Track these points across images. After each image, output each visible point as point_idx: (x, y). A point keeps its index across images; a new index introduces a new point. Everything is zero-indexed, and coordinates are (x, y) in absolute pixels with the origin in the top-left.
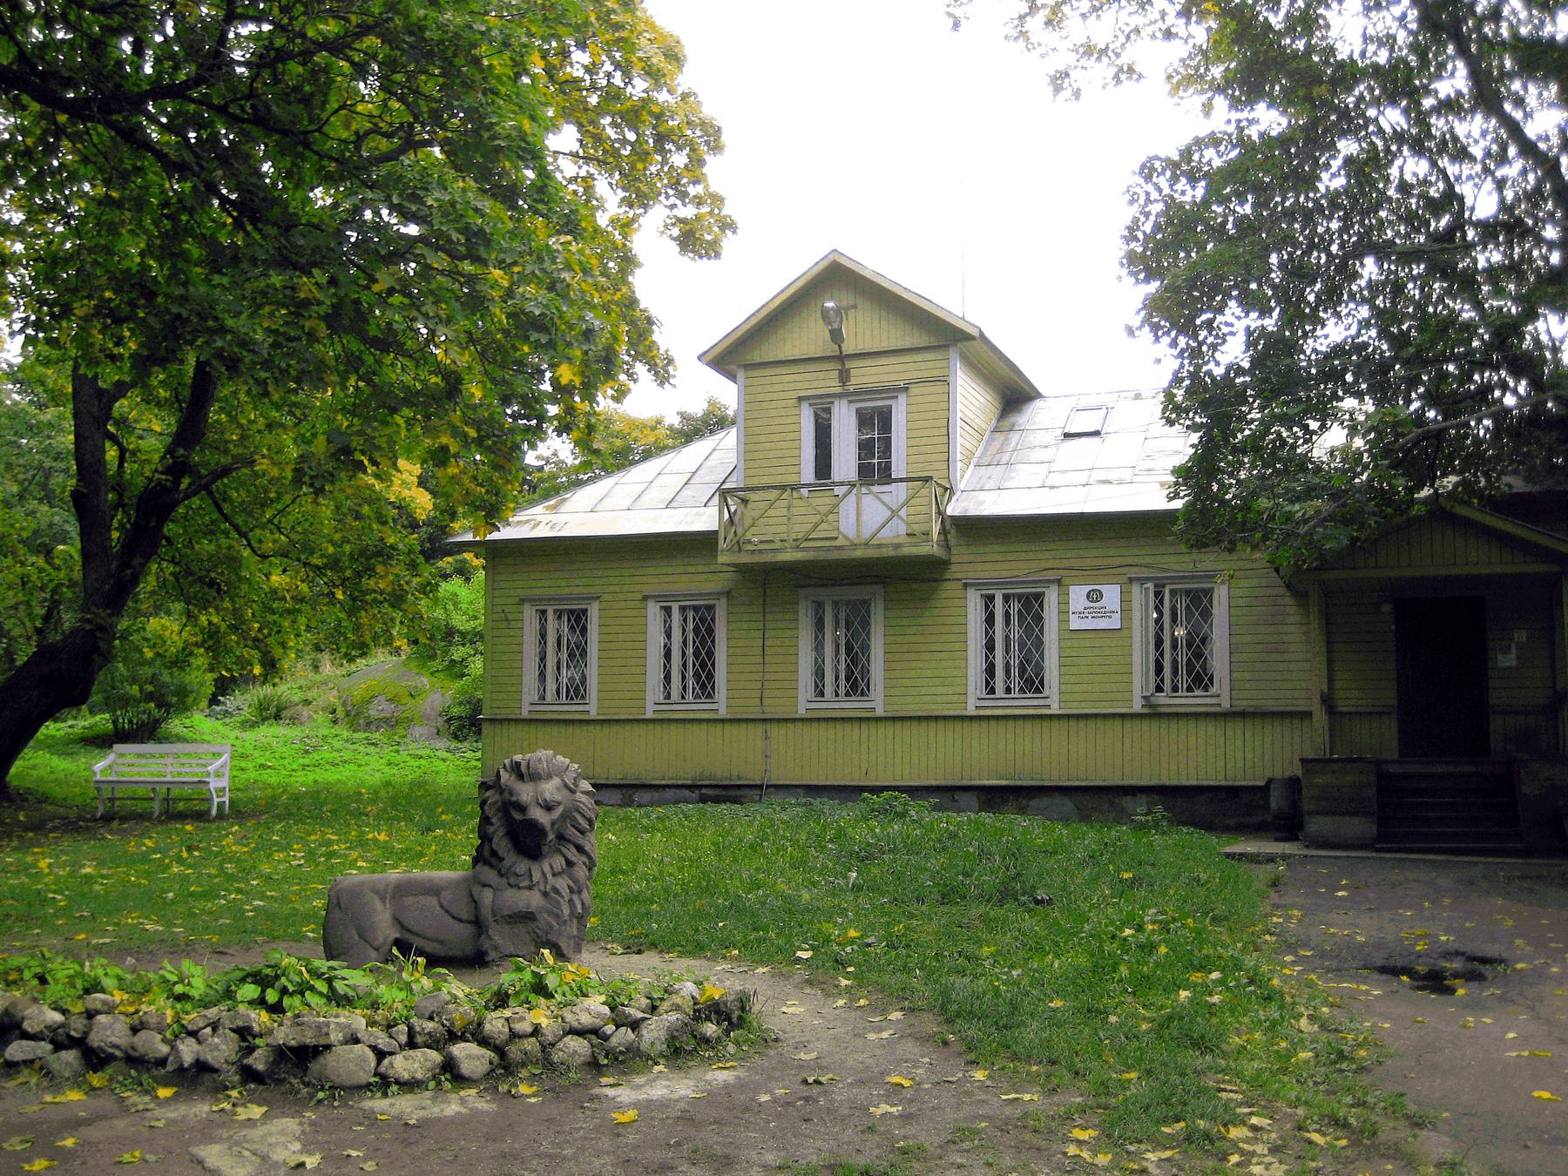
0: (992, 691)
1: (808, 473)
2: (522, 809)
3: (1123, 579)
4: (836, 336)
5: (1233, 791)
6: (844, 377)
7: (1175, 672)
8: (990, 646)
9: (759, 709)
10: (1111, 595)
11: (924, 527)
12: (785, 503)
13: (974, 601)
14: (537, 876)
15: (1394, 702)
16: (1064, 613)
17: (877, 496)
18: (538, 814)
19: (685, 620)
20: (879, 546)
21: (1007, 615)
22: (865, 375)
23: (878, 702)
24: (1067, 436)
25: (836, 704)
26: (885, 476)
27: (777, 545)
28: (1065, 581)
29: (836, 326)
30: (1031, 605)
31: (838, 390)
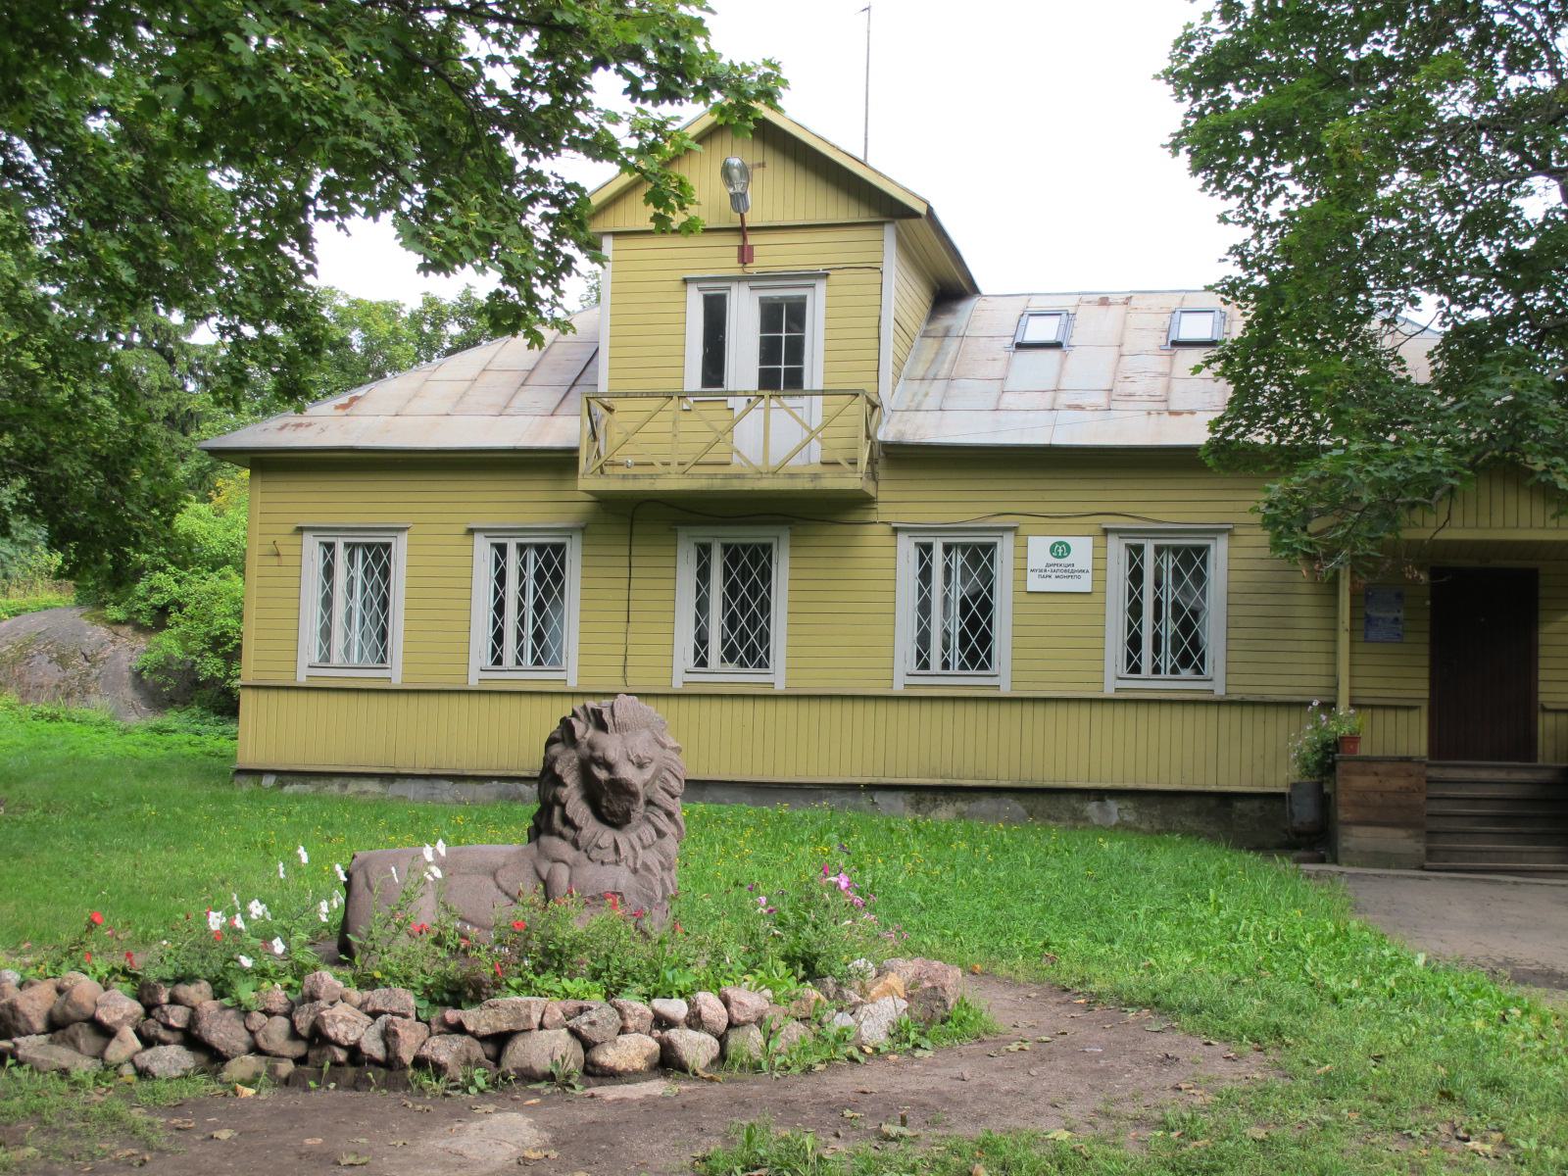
0: (926, 666)
1: (693, 379)
2: (609, 767)
3: (1094, 529)
4: (738, 201)
5: (1226, 798)
6: (745, 255)
7: (1157, 648)
8: (925, 608)
9: (621, 681)
10: (1082, 549)
11: (850, 454)
12: (669, 416)
13: (907, 550)
14: (624, 848)
15: (1426, 695)
16: (1022, 570)
17: (790, 410)
18: (627, 772)
19: (524, 563)
20: (792, 476)
21: (947, 570)
22: (770, 253)
23: (779, 675)
24: (1020, 346)
25: (723, 674)
26: (795, 381)
27: (660, 469)
28: (1023, 530)
29: (739, 189)
30: (980, 557)
31: (737, 272)
